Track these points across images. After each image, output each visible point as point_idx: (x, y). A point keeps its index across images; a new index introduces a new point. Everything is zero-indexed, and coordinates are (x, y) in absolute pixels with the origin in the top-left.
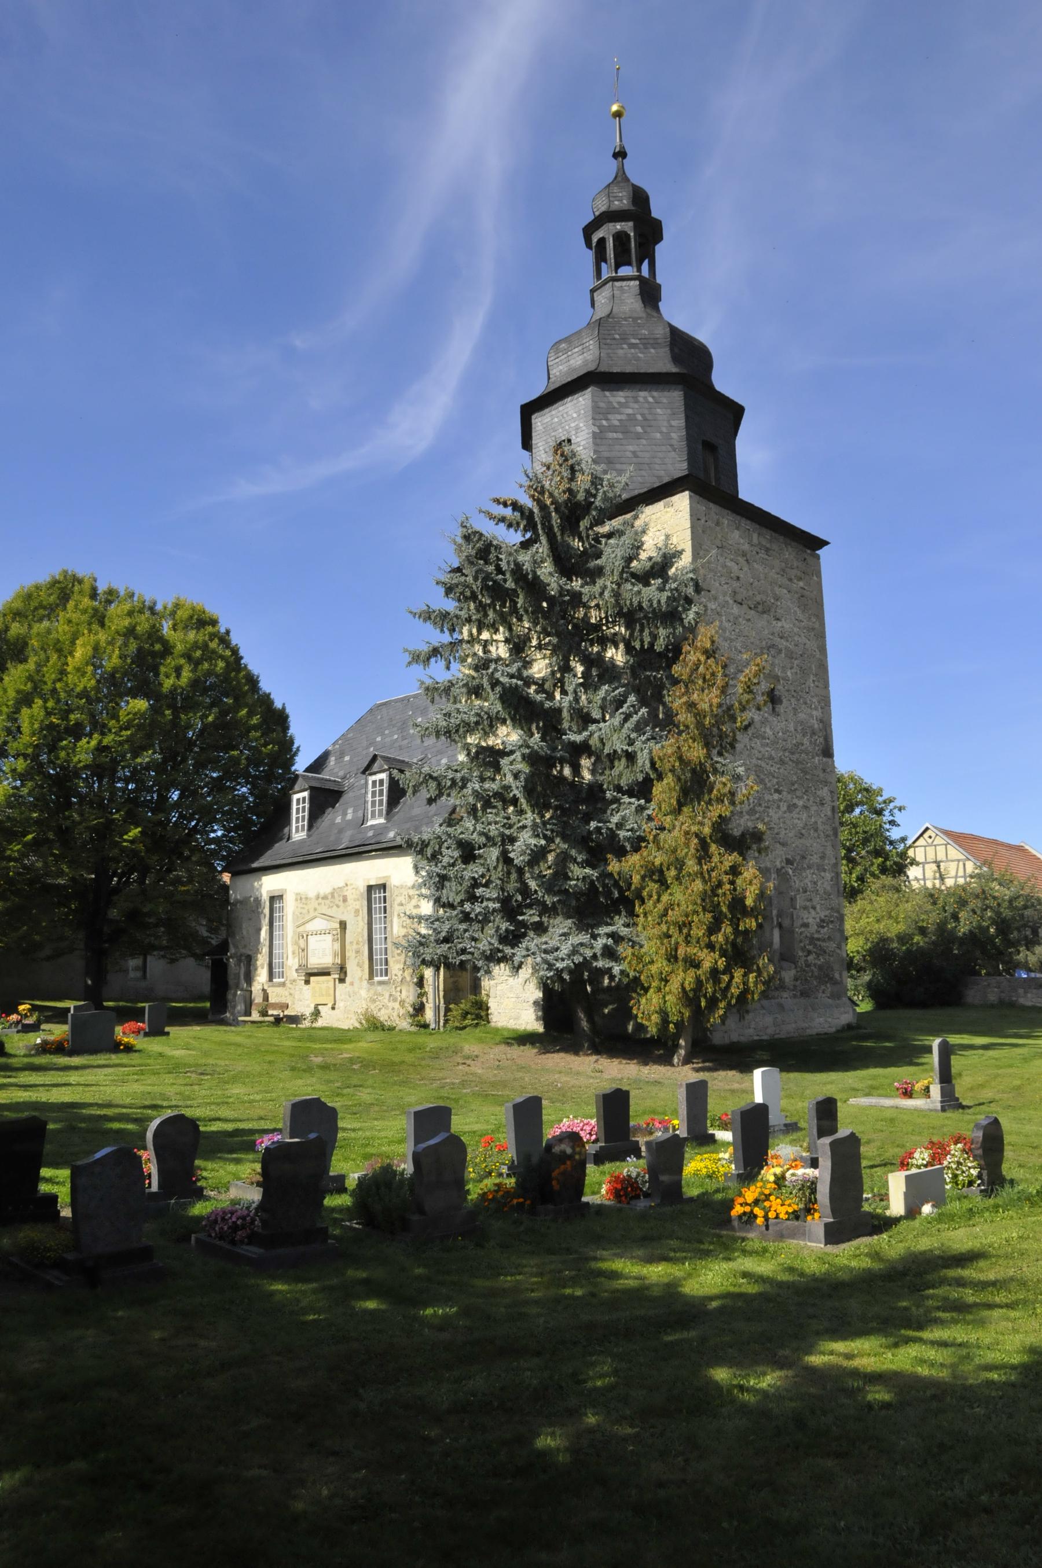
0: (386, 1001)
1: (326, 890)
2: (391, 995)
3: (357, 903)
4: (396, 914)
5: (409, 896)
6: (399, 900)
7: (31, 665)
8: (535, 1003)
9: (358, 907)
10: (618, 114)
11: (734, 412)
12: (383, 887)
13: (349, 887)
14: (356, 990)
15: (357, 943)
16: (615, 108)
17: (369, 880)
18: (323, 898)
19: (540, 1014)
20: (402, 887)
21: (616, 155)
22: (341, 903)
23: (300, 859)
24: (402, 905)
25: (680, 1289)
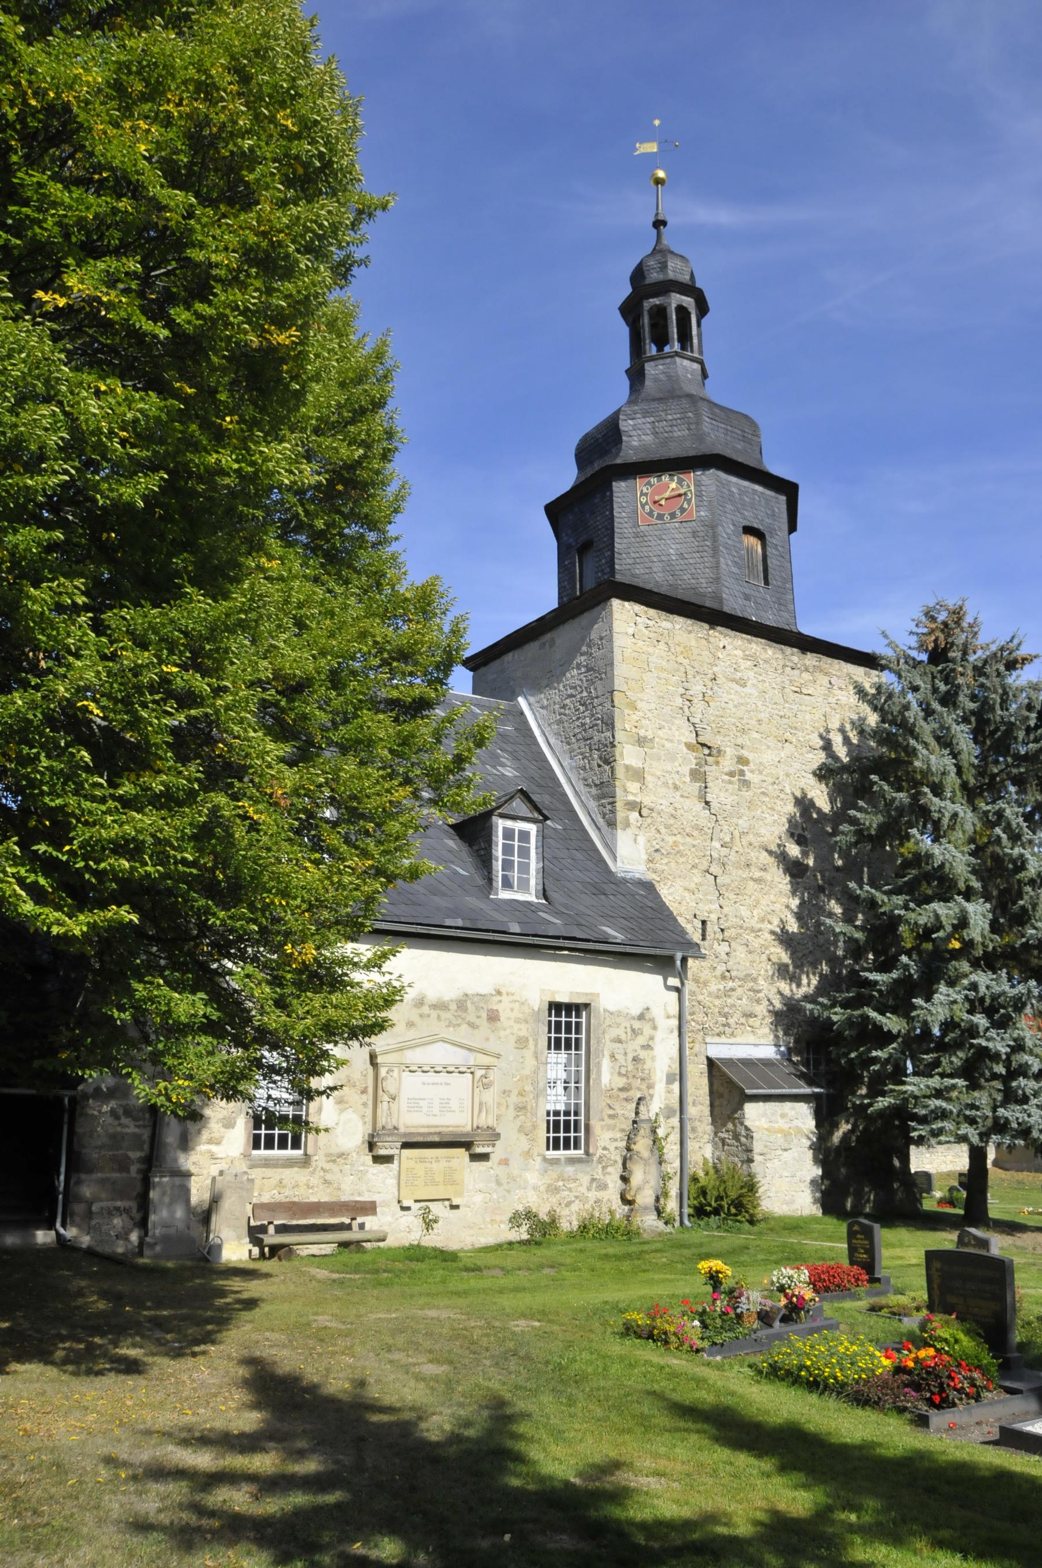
0: (583, 1189)
1: (450, 993)
2: (593, 1180)
3: (524, 1026)
4: (607, 1053)
5: (633, 1030)
6: (613, 1033)
7: (228, 311)
8: (813, 1182)
9: (524, 1033)
10: (658, 181)
11: (555, 511)
12: (587, 1006)
13: (504, 998)
14: (516, 1172)
15: (520, 1094)
16: (661, 174)
17: (554, 993)
18: (434, 1006)
19: (818, 1195)
20: (619, 1013)
21: (664, 223)
22: (483, 1022)
23: (420, 929)
24: (620, 1041)
25: (617, 1512)
